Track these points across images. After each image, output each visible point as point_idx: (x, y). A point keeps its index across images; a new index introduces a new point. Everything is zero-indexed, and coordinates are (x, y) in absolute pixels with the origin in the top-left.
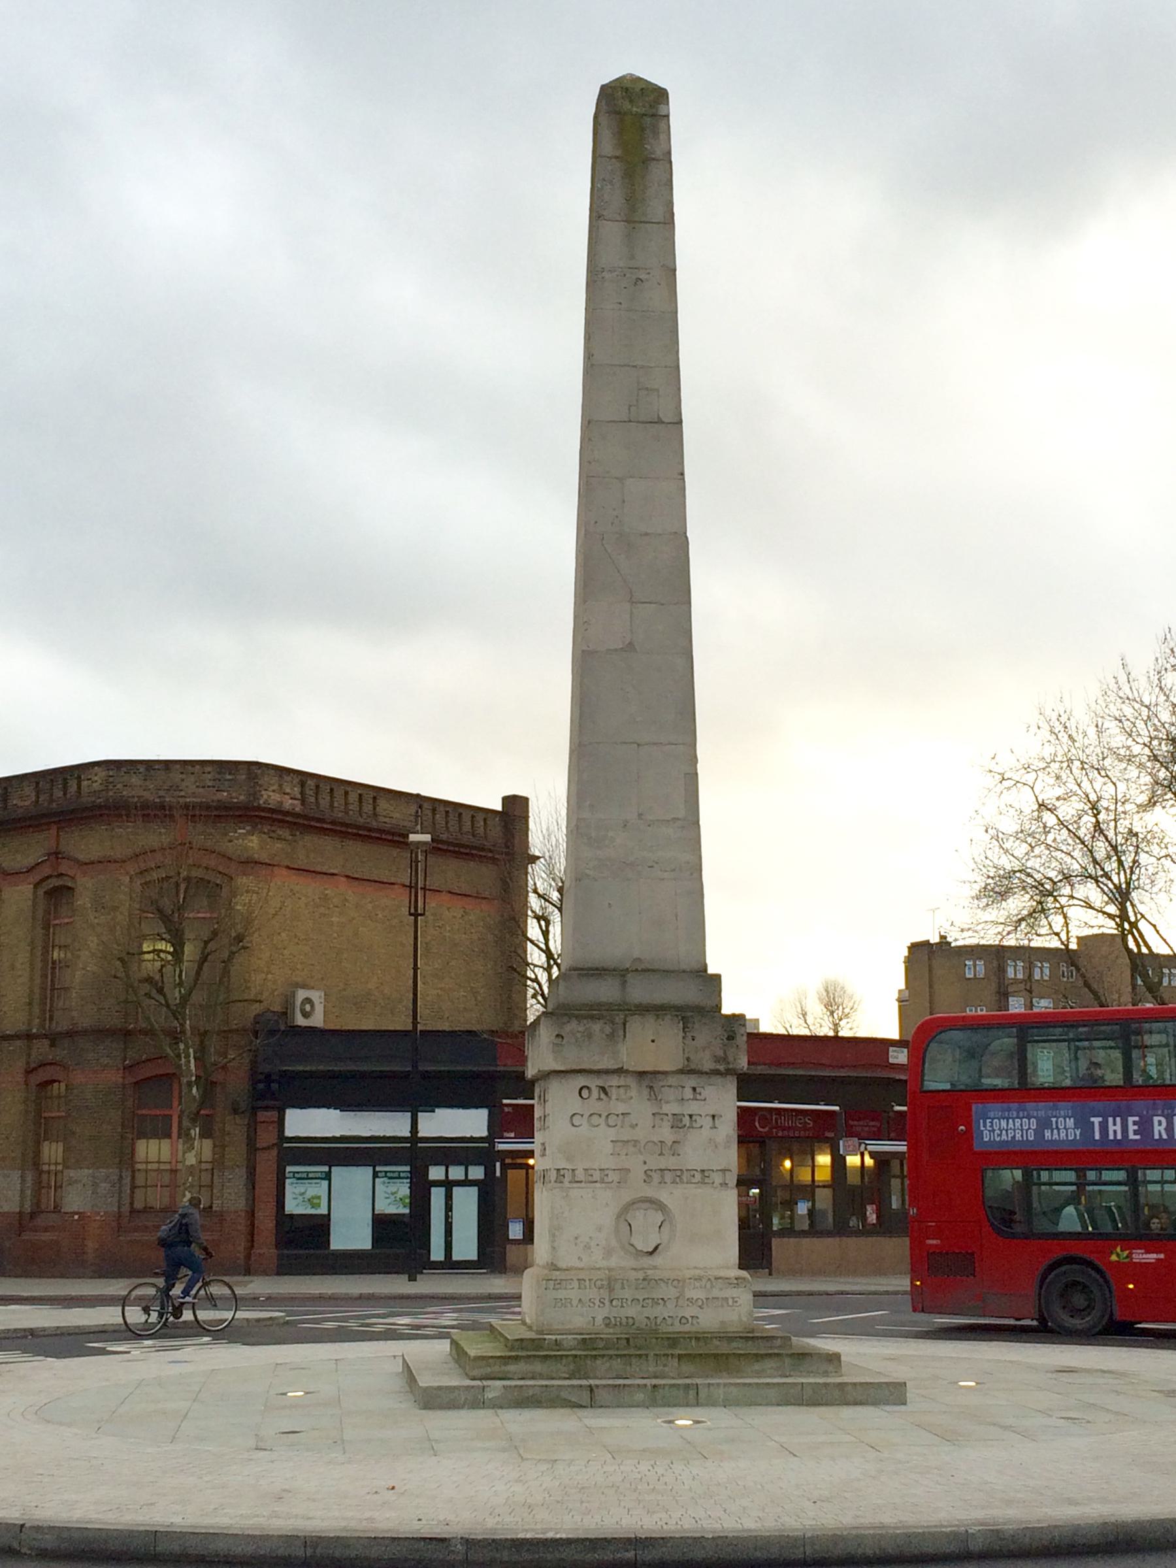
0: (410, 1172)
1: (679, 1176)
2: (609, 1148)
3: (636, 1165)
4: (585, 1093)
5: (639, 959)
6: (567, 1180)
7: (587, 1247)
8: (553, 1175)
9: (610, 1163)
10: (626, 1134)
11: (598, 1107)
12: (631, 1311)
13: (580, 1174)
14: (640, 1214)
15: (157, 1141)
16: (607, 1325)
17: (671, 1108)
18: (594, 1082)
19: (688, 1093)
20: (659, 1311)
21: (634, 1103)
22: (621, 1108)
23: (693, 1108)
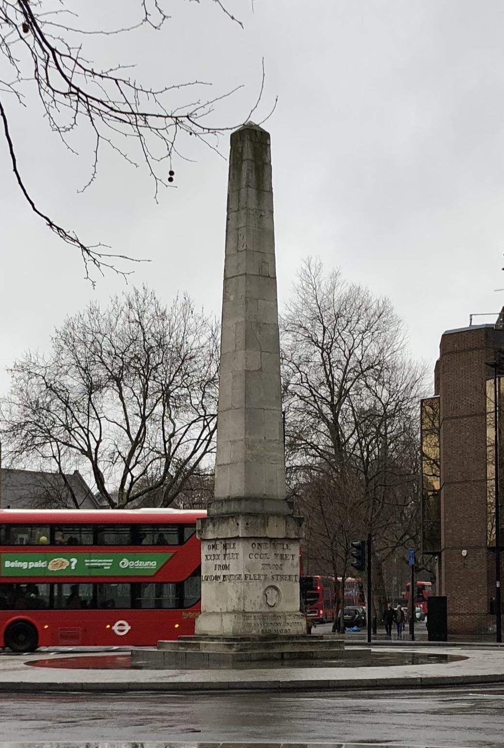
0: (130, 531)
1: (282, 577)
2: (261, 567)
3: (269, 572)
4: (254, 546)
5: (265, 495)
6: (248, 579)
7: (254, 604)
8: (243, 577)
9: (261, 572)
10: (266, 561)
11: (257, 551)
12: (270, 628)
13: (252, 577)
14: (270, 591)
15: (185, 601)
16: (263, 633)
17: (279, 552)
18: (257, 542)
19: (285, 547)
20: (279, 628)
21: (267, 550)
22: (264, 551)
23: (287, 552)
